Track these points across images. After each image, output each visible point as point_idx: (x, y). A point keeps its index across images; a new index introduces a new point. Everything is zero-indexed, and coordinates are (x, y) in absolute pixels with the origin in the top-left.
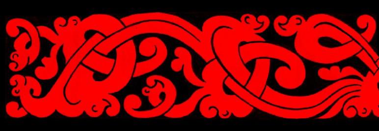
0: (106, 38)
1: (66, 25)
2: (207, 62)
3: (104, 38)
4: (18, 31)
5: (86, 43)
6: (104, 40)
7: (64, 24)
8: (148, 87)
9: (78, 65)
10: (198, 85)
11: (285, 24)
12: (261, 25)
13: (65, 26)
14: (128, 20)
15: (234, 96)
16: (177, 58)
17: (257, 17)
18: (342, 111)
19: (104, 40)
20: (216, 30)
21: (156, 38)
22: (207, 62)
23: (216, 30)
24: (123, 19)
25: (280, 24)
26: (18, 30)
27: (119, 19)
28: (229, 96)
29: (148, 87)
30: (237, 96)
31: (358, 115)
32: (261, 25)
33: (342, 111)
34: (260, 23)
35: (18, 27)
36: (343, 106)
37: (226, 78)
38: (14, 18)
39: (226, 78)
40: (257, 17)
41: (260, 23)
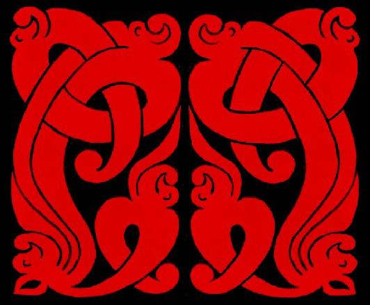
0: (117, 47)
1: (233, 35)
3: (114, 46)
6: (302, 82)
7: (233, 32)
8: (146, 26)
11: (208, 31)
13: (24, 265)
15: (302, 44)
16: (242, 27)
18: (203, 162)
19: (302, 82)
26: (131, 25)
28: (311, 43)
29: (146, 26)
30: (298, 44)
31: (198, 262)
33: (203, 162)
34: (30, 24)
36: (38, 133)
37: (331, 119)
39: (331, 119)
41: (30, 24)
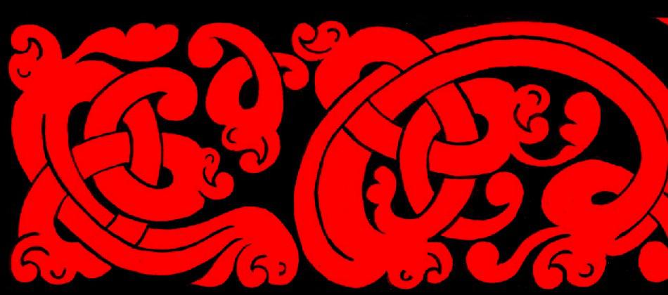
2: (435, 141)
4: (219, 52)
5: (387, 122)
9: (432, 142)
10: (316, 60)
11: (257, 153)
12: (33, 44)
14: (439, 41)
17: (544, 115)
20: (560, 253)
21: (308, 81)
22: (435, 141)
23: (560, 253)
24: (429, 41)
25: (260, 162)
27: (422, 38)
32: (33, 44)
35: (386, 274)
38: (364, 27)
40: (544, 115)
41: (256, 267)
